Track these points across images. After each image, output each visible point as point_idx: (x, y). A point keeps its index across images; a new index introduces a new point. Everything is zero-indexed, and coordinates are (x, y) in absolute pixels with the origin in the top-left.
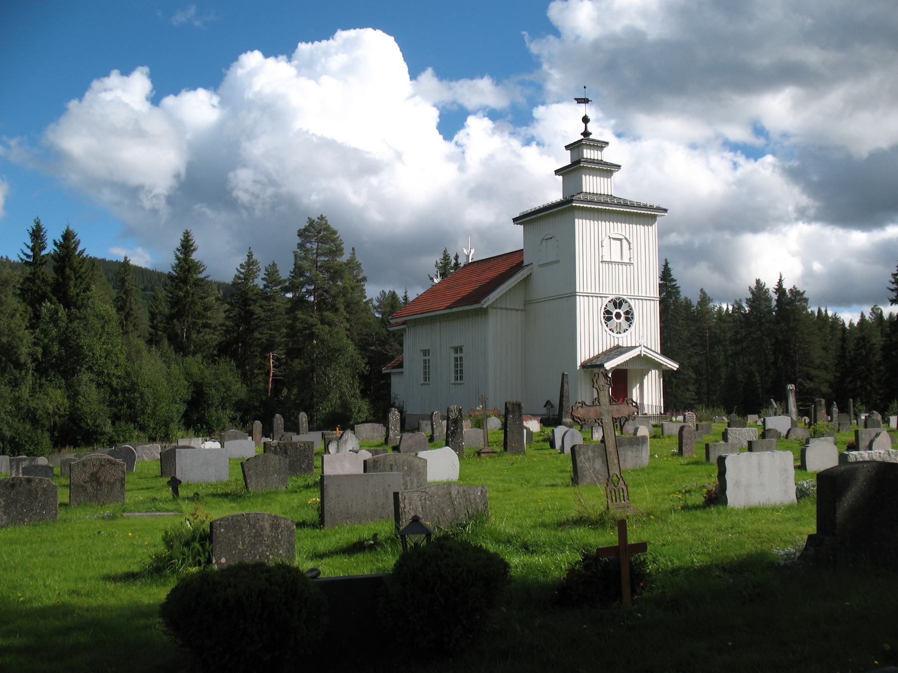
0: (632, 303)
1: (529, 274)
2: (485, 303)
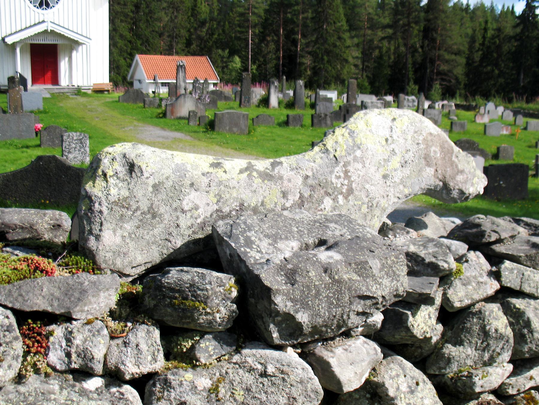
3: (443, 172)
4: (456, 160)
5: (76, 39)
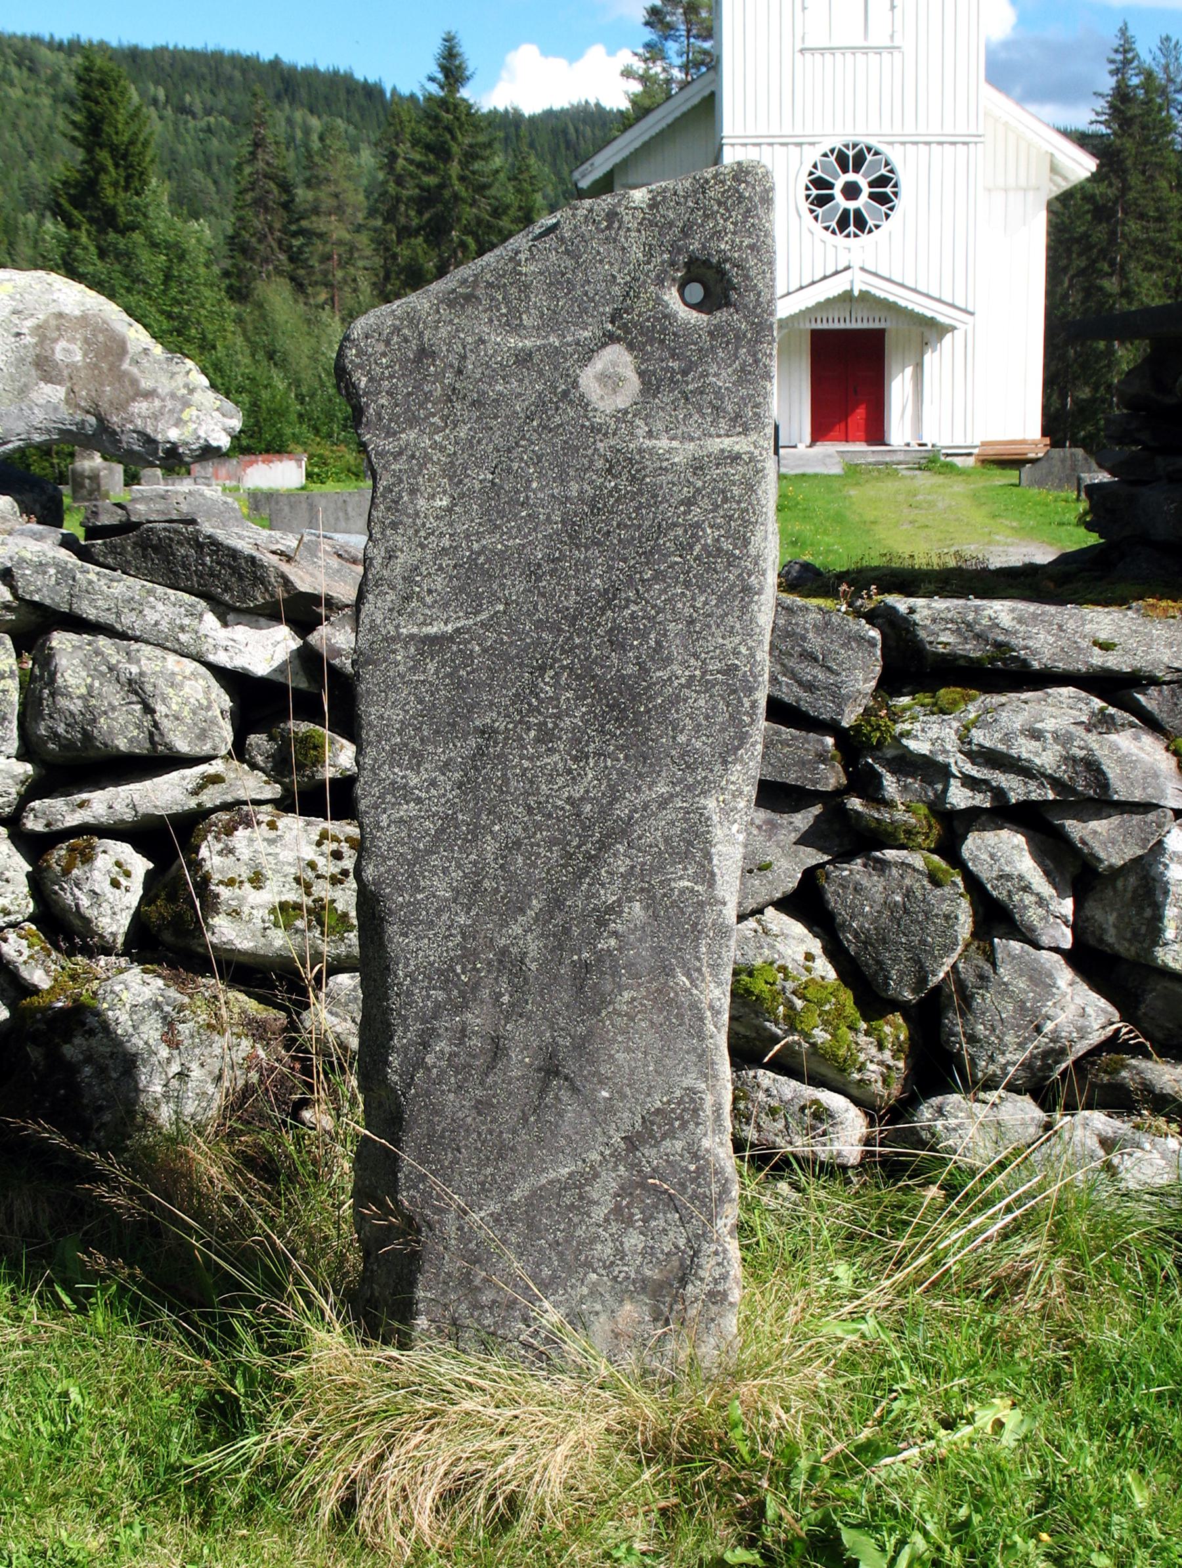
0: (895, 155)
1: (706, 93)
2: (584, 176)
3: (93, 394)
4: (134, 370)
5: (929, 314)
